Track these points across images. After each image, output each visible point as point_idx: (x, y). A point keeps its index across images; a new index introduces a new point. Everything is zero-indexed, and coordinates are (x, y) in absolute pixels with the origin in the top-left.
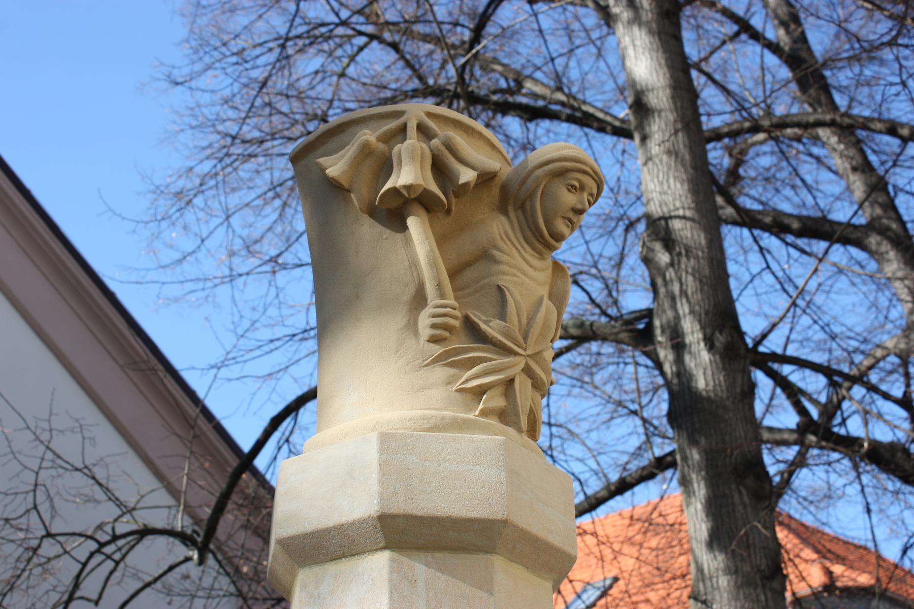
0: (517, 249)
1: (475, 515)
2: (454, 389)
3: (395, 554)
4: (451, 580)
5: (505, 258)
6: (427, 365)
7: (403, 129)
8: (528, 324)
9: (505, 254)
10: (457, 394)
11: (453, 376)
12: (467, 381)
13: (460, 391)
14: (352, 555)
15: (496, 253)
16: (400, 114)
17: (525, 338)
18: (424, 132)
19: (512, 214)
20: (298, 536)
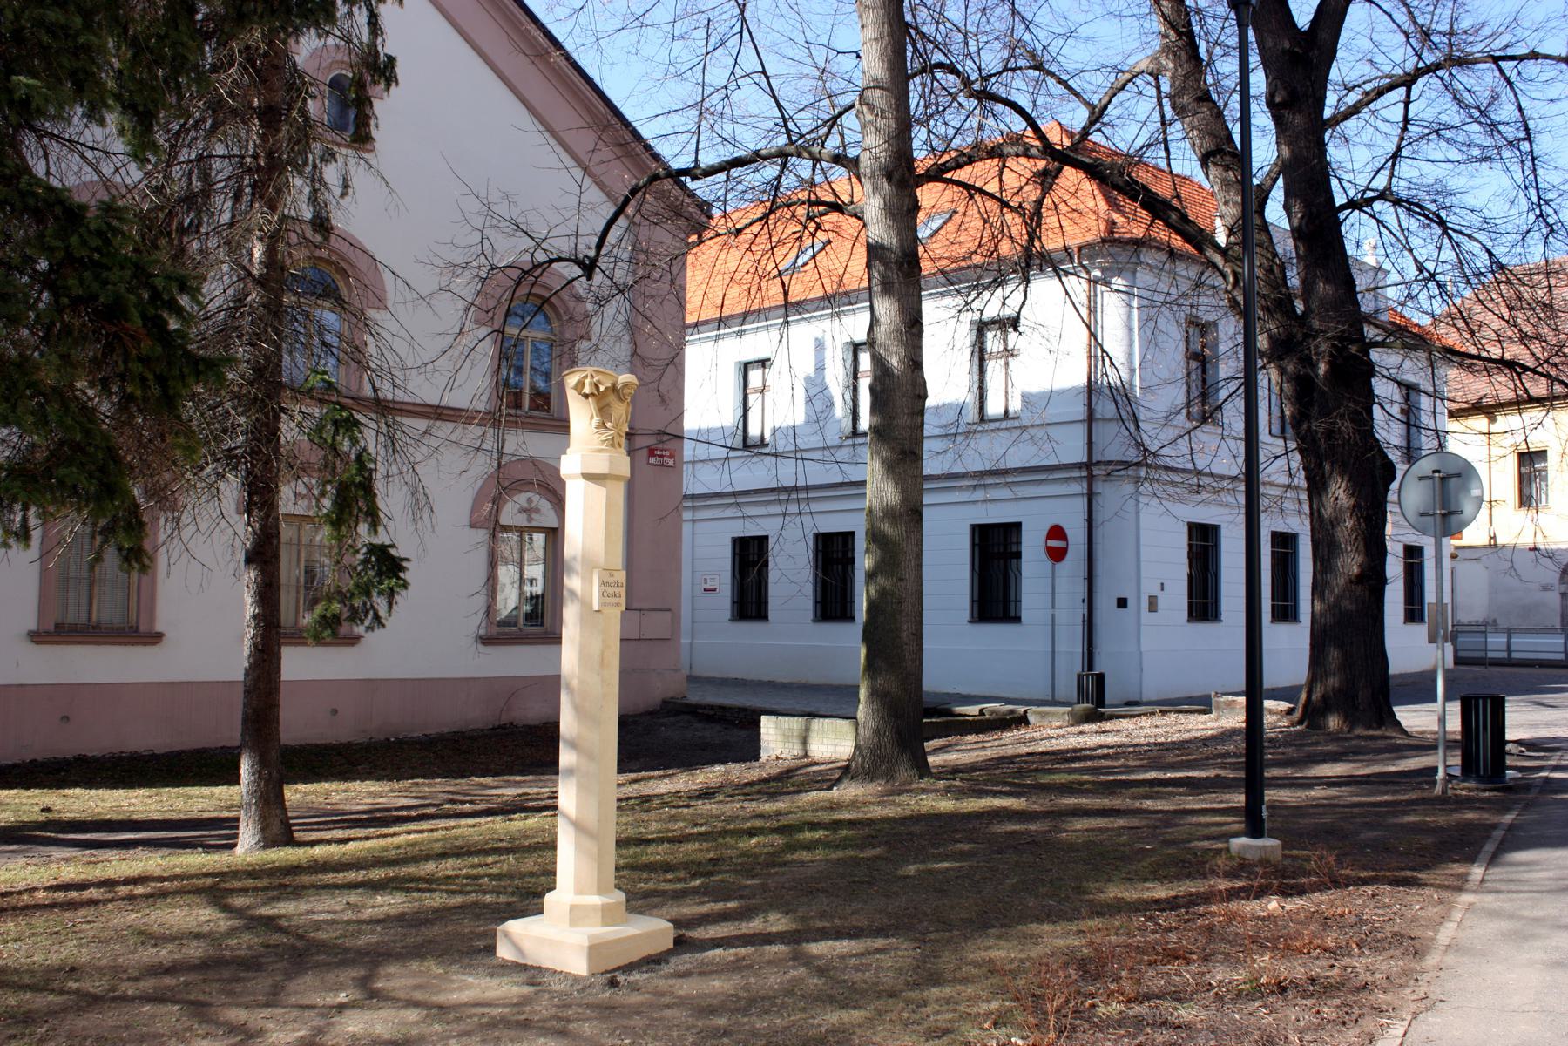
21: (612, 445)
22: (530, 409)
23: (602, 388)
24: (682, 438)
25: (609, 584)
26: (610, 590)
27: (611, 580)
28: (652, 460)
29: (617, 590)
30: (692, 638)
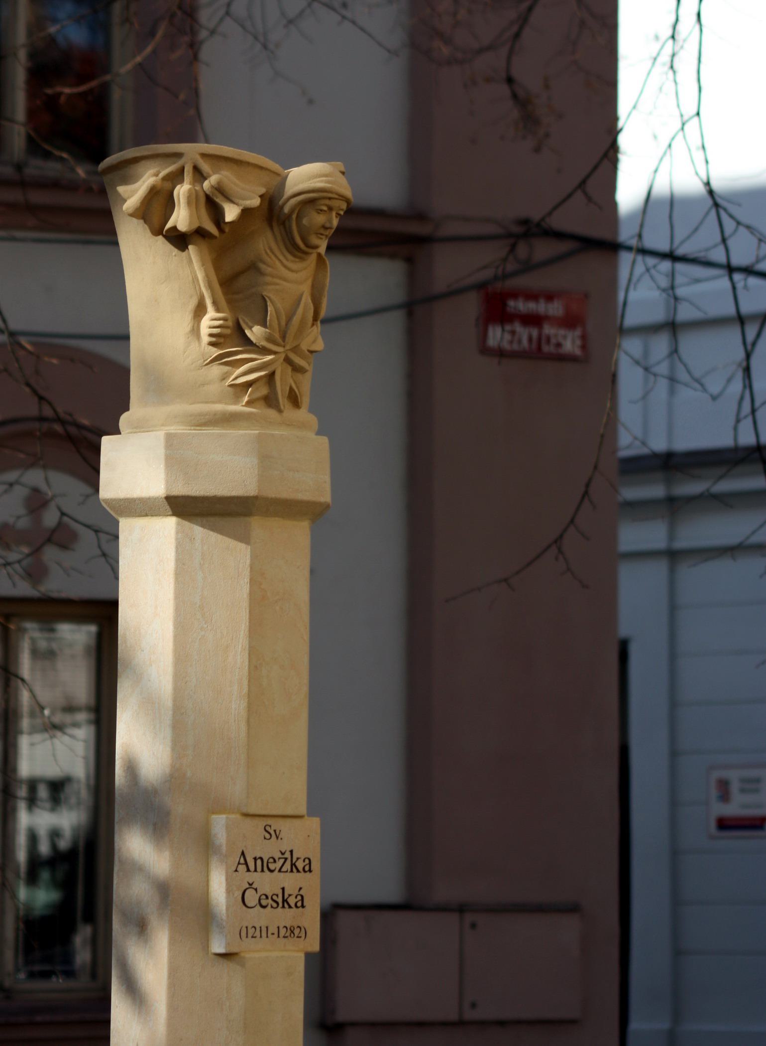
0: (279, 260)
1: (234, 493)
2: (227, 384)
3: (180, 520)
4: (219, 537)
5: (269, 270)
6: (207, 364)
7: (181, 171)
8: (286, 325)
9: (269, 266)
10: (229, 389)
11: (226, 373)
12: (236, 378)
13: (231, 386)
14: (152, 516)
15: (262, 266)
16: (178, 155)
17: (284, 337)
18: (199, 175)
19: (276, 229)
20: (115, 499)
21: (270, 401)
22: (34, 147)
23: (231, 213)
24: (612, 247)
25: (264, 865)
26: (268, 883)
27: (269, 850)
28: (496, 336)
29: (291, 882)
30: (677, 1016)
